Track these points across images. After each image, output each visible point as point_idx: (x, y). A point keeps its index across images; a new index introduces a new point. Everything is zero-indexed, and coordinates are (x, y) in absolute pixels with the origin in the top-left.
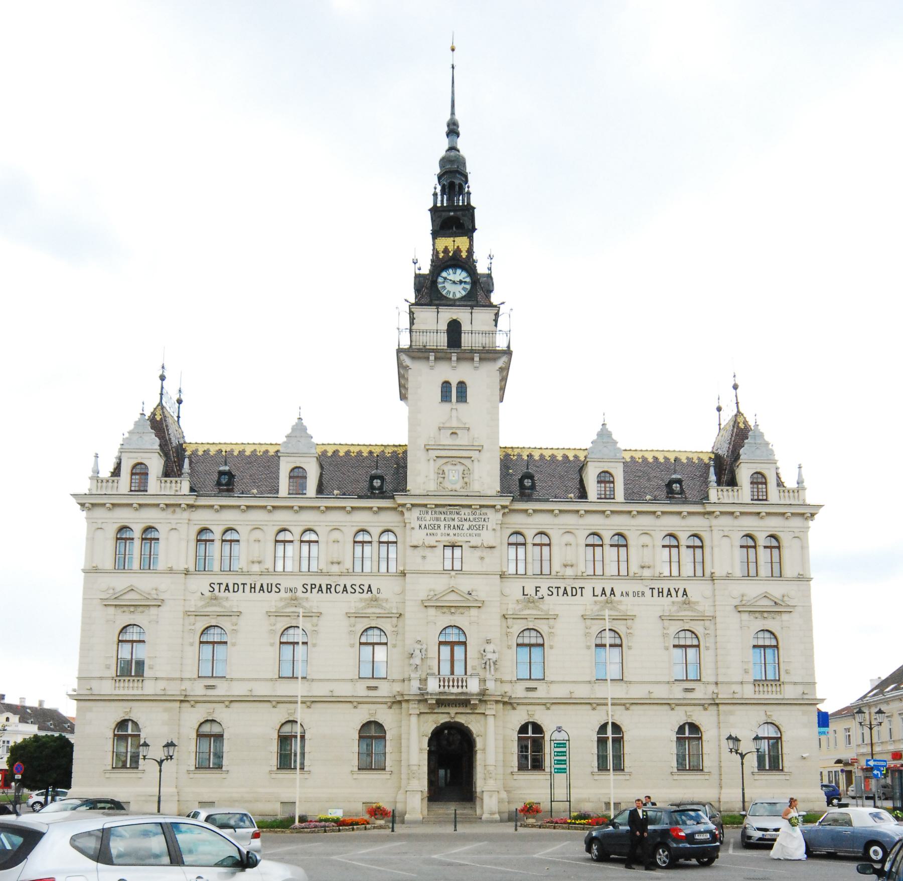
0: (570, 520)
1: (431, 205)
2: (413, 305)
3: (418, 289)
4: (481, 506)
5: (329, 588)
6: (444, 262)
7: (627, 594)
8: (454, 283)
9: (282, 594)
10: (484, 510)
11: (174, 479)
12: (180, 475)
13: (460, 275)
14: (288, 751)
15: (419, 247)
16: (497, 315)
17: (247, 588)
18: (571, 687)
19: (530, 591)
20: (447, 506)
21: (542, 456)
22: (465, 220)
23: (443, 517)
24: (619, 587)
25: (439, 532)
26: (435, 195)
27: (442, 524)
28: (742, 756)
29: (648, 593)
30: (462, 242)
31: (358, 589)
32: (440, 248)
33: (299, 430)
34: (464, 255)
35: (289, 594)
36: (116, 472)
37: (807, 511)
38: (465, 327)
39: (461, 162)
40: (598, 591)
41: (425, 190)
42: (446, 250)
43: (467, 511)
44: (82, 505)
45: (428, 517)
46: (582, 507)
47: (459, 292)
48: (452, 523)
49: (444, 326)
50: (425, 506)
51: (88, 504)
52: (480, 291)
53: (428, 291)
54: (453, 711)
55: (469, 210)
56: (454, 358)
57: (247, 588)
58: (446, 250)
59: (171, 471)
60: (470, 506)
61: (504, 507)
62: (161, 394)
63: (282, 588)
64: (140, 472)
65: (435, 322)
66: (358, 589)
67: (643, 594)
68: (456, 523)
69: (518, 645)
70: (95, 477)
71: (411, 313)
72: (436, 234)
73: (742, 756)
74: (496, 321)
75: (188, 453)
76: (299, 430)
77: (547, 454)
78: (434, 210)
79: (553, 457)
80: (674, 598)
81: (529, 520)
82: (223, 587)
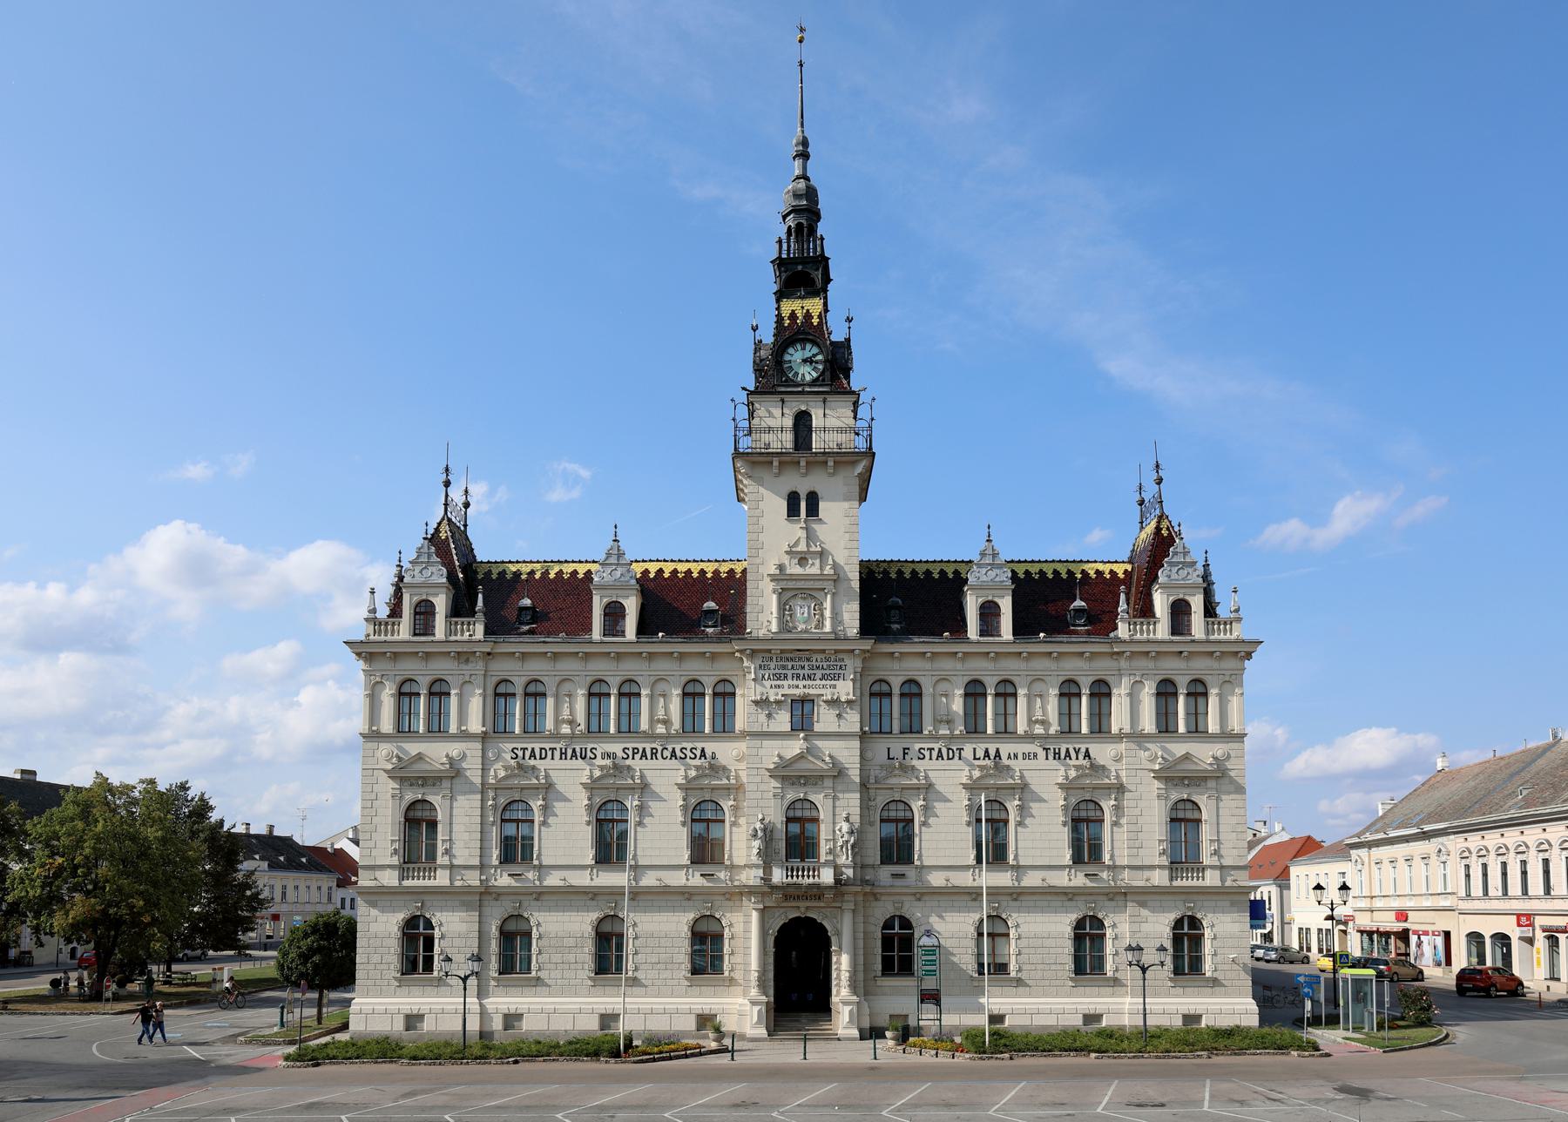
0: (947, 665)
1: (776, 255)
2: (752, 393)
3: (759, 370)
4: (836, 651)
5: (654, 753)
6: (792, 334)
7: (1016, 756)
8: (803, 363)
9: (599, 761)
10: (840, 656)
11: (466, 620)
12: (472, 613)
13: (810, 350)
14: (608, 953)
15: (758, 308)
16: (856, 404)
17: (557, 754)
18: (950, 874)
19: (897, 752)
20: (789, 655)
21: (914, 572)
22: (818, 276)
23: (790, 664)
24: (1006, 749)
25: (785, 683)
26: (780, 242)
27: (790, 673)
28: (1144, 970)
29: (1042, 754)
30: (814, 305)
31: (689, 754)
32: (786, 312)
33: (616, 554)
34: (815, 321)
35: (608, 762)
36: (396, 611)
37: (1243, 648)
38: (816, 422)
39: (815, 191)
40: (980, 754)
41: (768, 233)
42: (793, 316)
43: (819, 657)
44: (359, 654)
45: (772, 665)
46: (961, 648)
47: (808, 373)
48: (801, 672)
49: (789, 422)
50: (769, 651)
51: (365, 651)
52: (837, 367)
53: (771, 376)
54: (803, 904)
55: (823, 261)
56: (803, 463)
57: (557, 754)
58: (793, 316)
59: (461, 609)
60: (823, 651)
61: (864, 651)
62: (446, 505)
63: (599, 754)
64: (424, 612)
65: (776, 419)
66: (689, 754)
67: (1035, 756)
68: (806, 672)
69: (882, 821)
70: (373, 620)
71: (750, 404)
72: (780, 296)
73: (1144, 970)
74: (855, 412)
75: (480, 576)
76: (616, 554)
77: (921, 569)
78: (780, 263)
79: (928, 573)
80: (1074, 762)
81: (896, 665)
82: (528, 754)
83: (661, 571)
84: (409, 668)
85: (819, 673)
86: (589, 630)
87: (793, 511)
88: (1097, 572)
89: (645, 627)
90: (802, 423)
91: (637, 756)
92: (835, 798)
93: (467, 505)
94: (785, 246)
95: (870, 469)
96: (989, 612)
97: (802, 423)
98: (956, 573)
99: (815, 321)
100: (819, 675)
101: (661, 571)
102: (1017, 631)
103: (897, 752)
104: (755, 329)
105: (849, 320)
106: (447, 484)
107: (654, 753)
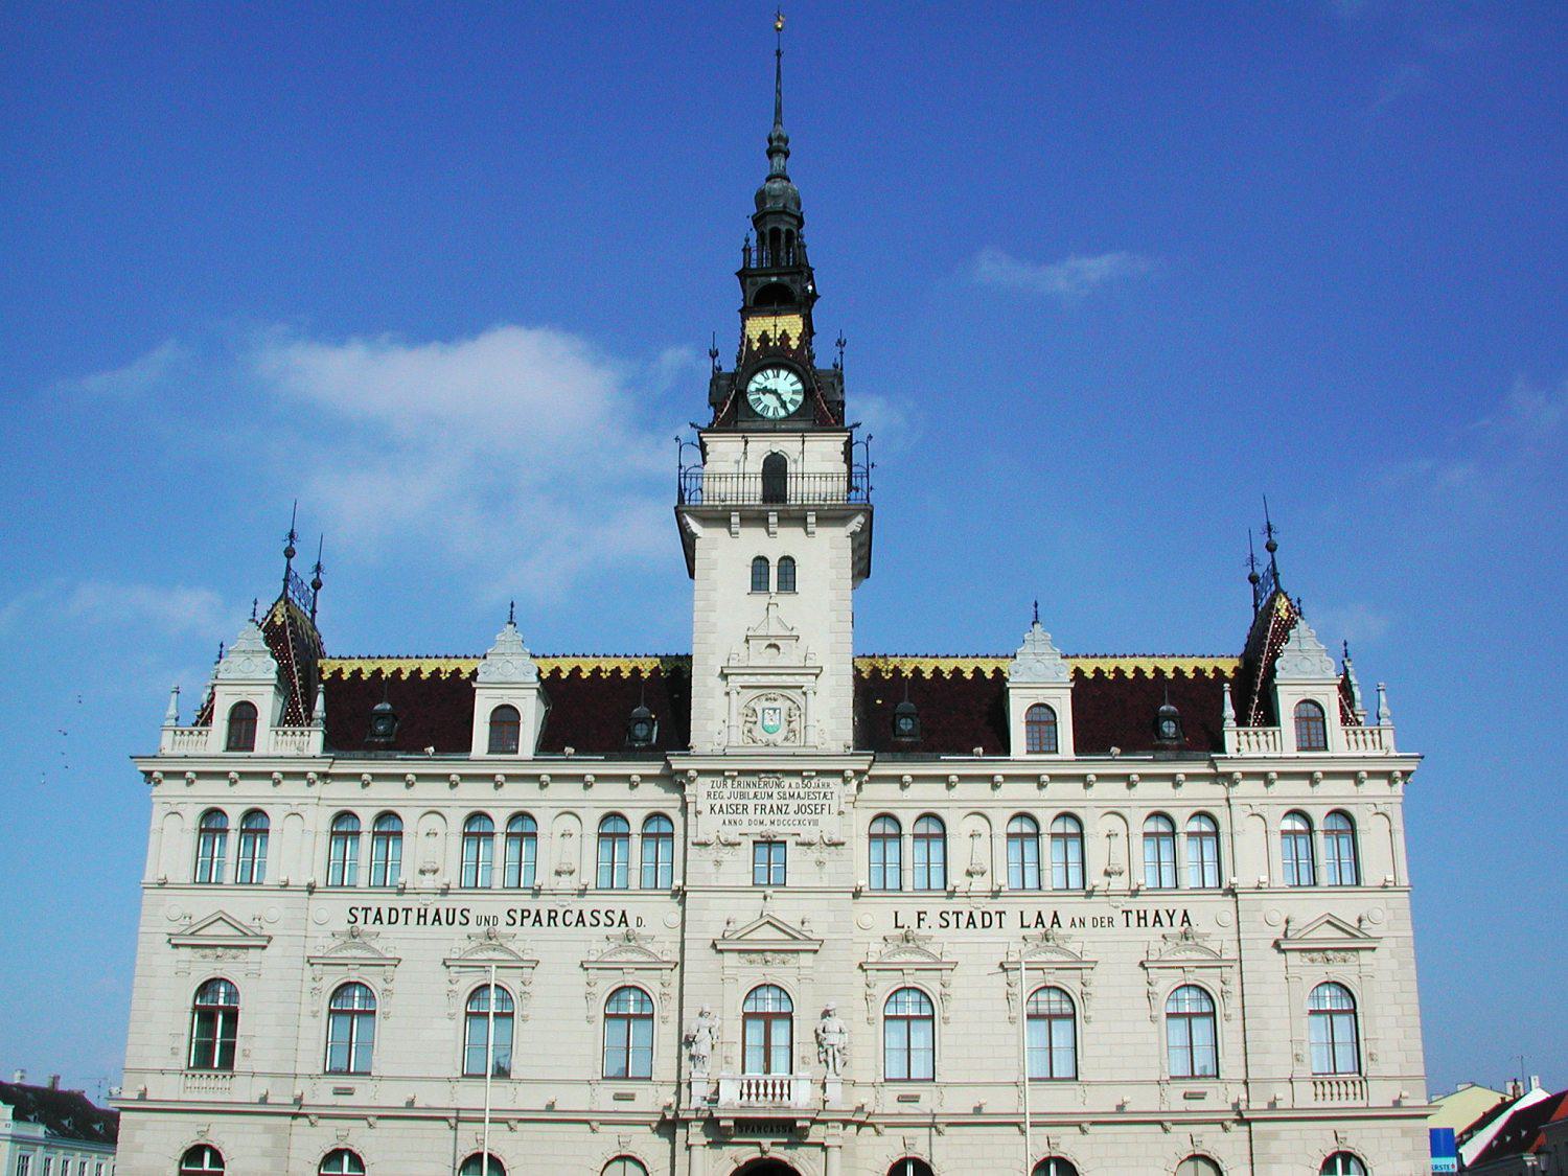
7: (1082, 922)
9: (472, 928)
17: (413, 916)
23: (751, 792)
25: (745, 818)
27: (751, 804)
29: (1120, 919)
34: (794, 344)
40: (1030, 919)
42: (764, 338)
48: (768, 802)
57: (413, 916)
58: (764, 338)
62: (286, 580)
67: (1111, 922)
68: (775, 802)
75: (326, 676)
83: (577, 670)
84: (213, 792)
85: (793, 804)
86: (466, 746)
87: (759, 582)
88: (1196, 670)
89: (549, 744)
90: (775, 470)
91: (528, 922)
92: (746, 442)
93: (317, 585)
94: (754, 255)
95: (868, 528)
96: (1042, 719)
97: (775, 470)
98: (998, 672)
99: (794, 344)
100: (793, 807)
101: (577, 670)
102: (1078, 749)
103: (908, 918)
104: (826, 1014)
105: (841, 343)
106: (290, 553)
107: (552, 916)
